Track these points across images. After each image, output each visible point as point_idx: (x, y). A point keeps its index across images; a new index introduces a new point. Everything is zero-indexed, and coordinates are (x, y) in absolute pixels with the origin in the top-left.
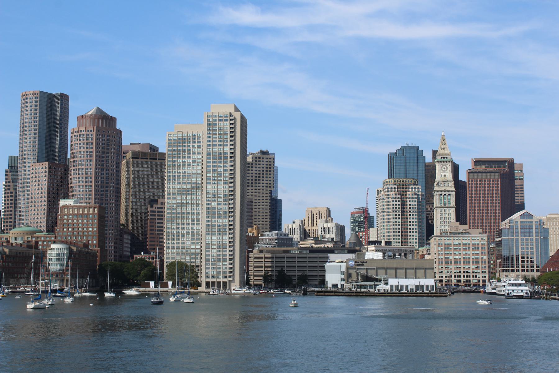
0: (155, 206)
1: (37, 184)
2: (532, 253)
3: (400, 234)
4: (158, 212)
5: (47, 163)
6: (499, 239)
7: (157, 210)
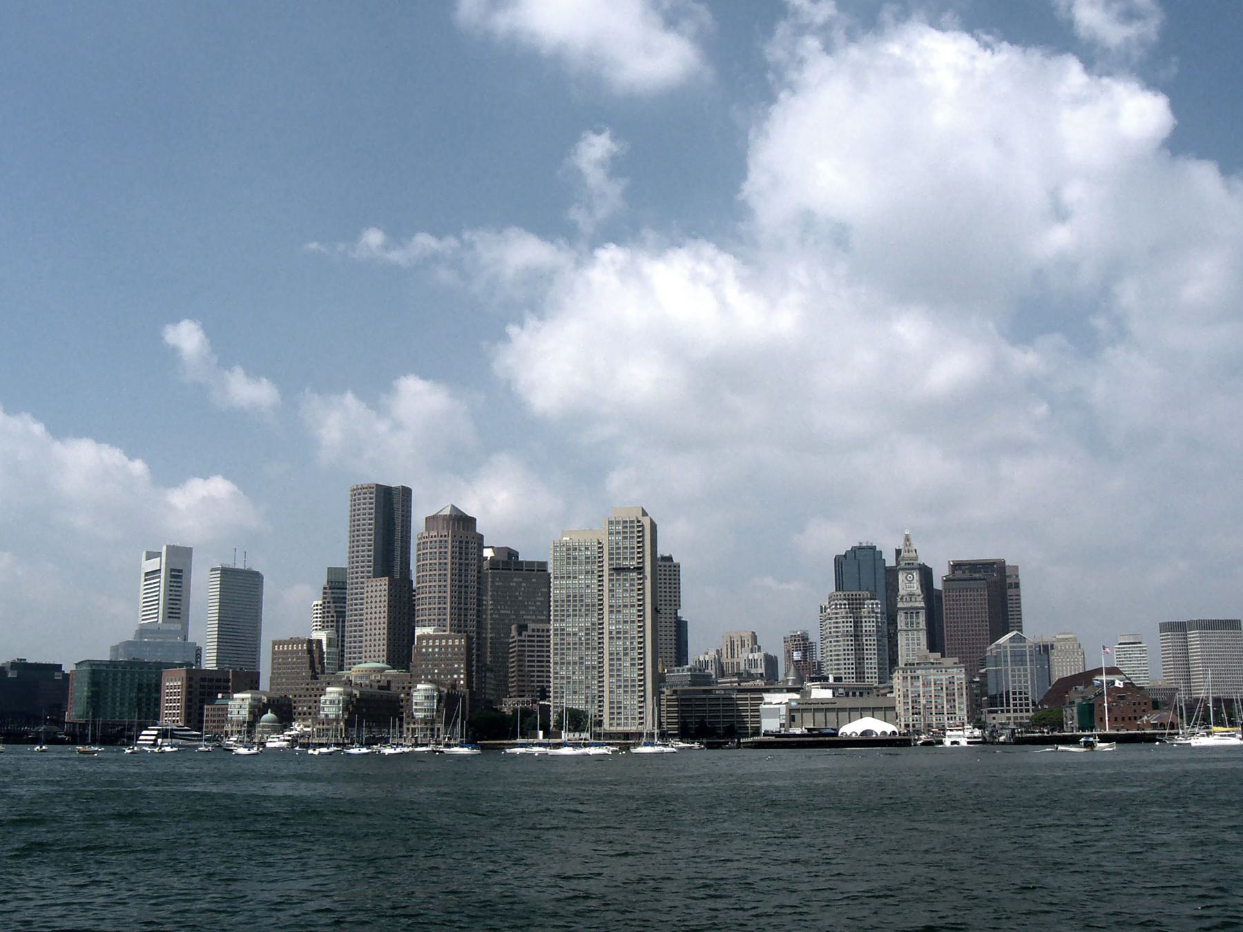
0: (524, 633)
1: (374, 606)
2: (1026, 687)
3: (854, 676)
4: (529, 641)
5: (387, 578)
6: (984, 670)
7: (527, 639)
